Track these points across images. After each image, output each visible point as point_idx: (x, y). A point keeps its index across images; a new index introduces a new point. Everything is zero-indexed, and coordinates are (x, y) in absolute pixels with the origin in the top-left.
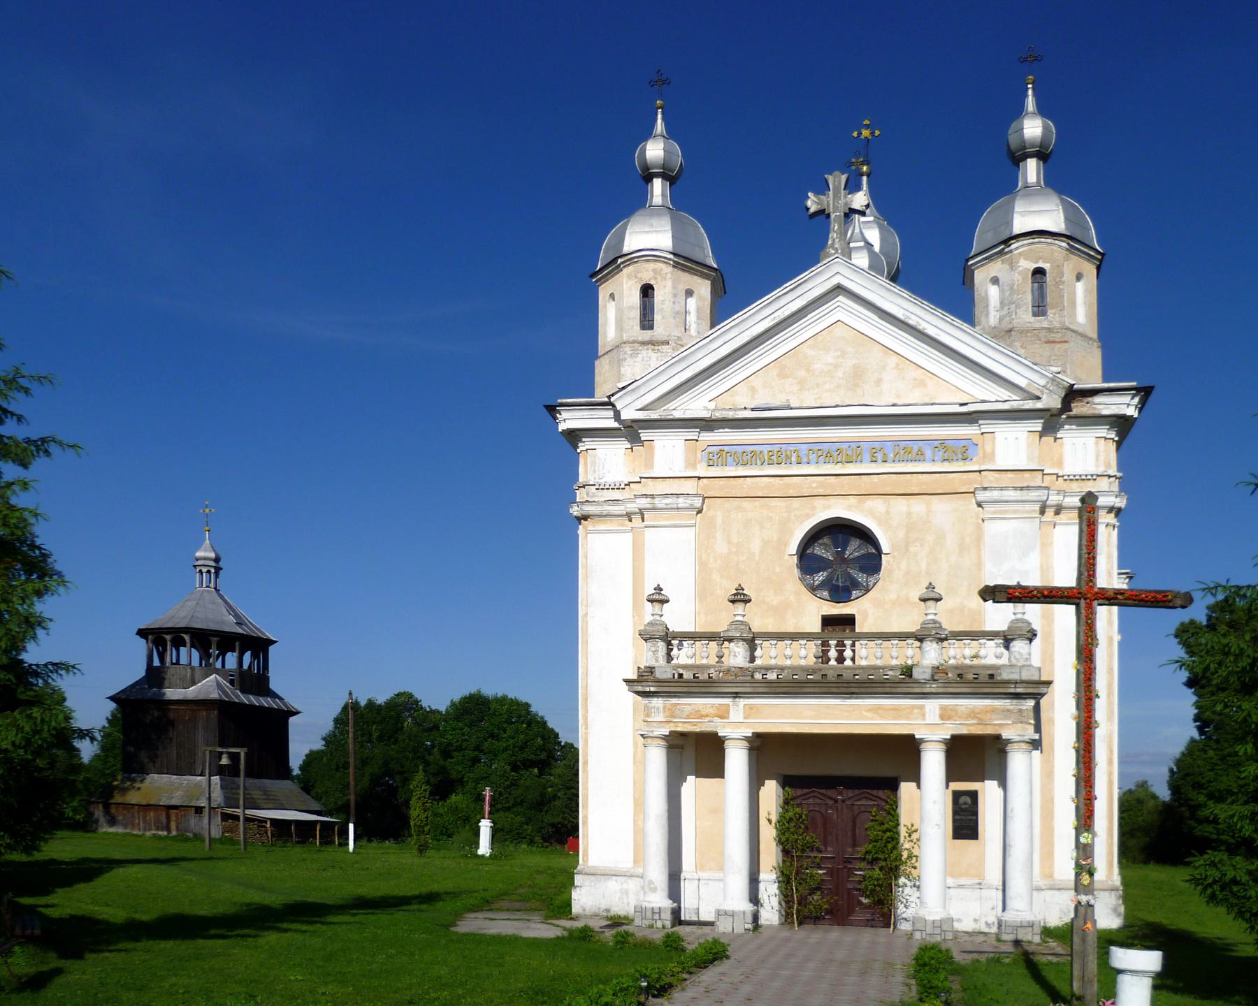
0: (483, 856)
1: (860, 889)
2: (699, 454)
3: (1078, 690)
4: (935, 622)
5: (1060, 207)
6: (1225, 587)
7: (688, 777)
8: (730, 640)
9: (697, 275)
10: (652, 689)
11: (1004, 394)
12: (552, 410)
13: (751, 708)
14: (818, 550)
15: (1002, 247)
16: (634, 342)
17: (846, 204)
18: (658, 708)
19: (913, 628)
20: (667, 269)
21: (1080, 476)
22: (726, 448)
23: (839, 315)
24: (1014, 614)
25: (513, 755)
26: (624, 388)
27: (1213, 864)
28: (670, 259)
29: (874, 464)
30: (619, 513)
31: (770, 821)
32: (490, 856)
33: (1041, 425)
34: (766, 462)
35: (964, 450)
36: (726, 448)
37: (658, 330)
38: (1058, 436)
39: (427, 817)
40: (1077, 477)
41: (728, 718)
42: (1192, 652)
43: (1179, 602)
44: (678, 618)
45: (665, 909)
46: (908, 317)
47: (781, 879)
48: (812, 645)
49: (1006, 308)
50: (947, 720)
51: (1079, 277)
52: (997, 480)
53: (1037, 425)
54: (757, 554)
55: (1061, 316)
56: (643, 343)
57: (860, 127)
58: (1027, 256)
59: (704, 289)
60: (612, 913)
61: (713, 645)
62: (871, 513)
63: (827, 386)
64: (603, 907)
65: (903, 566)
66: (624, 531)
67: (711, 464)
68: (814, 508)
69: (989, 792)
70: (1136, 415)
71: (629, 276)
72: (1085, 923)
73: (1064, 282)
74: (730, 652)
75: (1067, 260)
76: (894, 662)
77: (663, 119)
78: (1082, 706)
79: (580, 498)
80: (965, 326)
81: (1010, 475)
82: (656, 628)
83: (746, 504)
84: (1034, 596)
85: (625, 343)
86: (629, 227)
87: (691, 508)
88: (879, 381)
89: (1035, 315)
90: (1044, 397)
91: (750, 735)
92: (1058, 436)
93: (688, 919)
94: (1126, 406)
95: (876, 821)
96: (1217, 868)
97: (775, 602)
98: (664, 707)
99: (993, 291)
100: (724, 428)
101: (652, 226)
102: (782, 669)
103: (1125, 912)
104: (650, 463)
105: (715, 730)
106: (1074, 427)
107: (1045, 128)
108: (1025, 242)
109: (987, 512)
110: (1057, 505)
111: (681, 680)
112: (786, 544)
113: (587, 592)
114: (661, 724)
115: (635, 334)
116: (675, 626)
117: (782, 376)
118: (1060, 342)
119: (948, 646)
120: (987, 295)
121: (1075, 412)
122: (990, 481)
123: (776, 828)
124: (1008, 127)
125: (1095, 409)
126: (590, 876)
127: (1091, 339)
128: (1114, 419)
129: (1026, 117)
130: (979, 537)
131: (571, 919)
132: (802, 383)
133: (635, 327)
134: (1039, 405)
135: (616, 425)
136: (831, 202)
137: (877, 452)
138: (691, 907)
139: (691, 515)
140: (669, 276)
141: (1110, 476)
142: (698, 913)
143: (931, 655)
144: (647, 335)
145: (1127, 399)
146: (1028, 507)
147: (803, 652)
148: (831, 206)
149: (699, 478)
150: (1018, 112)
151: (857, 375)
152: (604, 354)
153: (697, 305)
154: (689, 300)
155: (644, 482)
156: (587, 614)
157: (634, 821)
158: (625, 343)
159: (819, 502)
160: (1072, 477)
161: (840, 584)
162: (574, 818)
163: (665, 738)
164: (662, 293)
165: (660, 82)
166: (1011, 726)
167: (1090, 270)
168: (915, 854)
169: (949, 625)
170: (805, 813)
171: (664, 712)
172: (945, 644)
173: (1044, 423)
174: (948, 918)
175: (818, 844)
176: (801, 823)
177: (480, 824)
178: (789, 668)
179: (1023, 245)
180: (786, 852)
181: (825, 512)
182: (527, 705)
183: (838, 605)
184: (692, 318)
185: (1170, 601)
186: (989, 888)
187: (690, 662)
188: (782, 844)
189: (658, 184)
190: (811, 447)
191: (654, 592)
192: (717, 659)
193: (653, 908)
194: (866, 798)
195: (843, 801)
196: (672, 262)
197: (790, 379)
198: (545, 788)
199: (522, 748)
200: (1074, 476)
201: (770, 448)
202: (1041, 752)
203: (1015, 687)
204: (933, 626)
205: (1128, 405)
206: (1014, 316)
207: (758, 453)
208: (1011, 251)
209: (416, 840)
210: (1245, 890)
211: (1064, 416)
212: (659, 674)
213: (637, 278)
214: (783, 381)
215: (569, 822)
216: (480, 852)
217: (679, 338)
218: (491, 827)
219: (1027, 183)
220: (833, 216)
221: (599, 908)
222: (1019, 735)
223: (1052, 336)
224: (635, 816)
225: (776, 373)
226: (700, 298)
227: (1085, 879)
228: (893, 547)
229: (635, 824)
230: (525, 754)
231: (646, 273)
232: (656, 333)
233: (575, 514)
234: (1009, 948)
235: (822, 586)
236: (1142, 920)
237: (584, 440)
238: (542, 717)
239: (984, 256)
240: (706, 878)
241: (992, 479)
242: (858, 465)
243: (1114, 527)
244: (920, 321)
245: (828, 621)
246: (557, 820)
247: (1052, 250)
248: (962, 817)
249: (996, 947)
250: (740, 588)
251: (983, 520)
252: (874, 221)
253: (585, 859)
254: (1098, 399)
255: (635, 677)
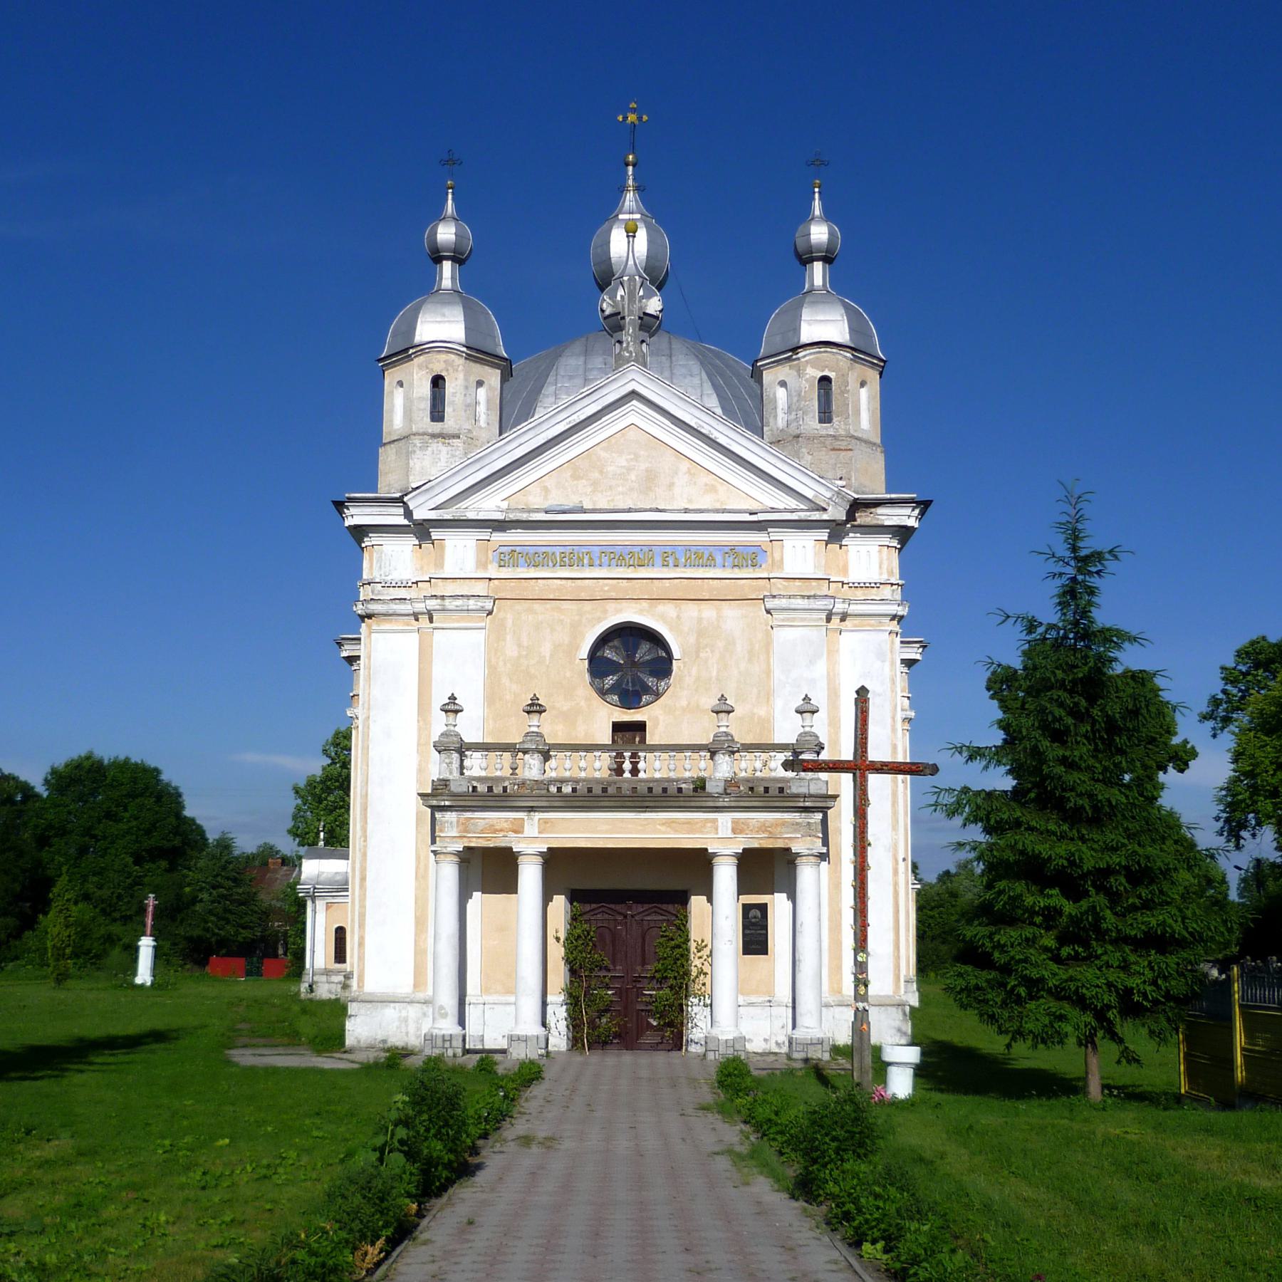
0: (142, 986)
1: (649, 1011)
2: (490, 553)
3: (855, 841)
4: (727, 734)
5: (845, 318)
6: (968, 747)
7: (474, 893)
8: (525, 752)
9: (488, 365)
10: (447, 803)
11: (792, 503)
12: (340, 506)
13: (546, 823)
14: (608, 654)
15: (790, 354)
16: (424, 434)
17: (641, 308)
18: (451, 823)
19: (706, 739)
20: (460, 362)
21: (865, 583)
22: (518, 549)
23: (632, 419)
24: (803, 727)
25: (137, 841)
26: (417, 488)
27: (960, 975)
28: (463, 352)
29: (665, 569)
30: (406, 612)
31: (558, 939)
32: (153, 984)
33: (827, 534)
34: (558, 564)
35: (752, 557)
36: (518, 549)
37: (449, 422)
38: (844, 543)
39: (69, 936)
40: (862, 585)
41: (522, 832)
42: (1006, 707)
43: (928, 771)
44: (470, 728)
45: (456, 1035)
46: (700, 426)
47: (569, 1001)
48: (606, 755)
49: (794, 413)
50: (738, 834)
51: (863, 384)
52: (786, 588)
53: (824, 535)
54: (548, 658)
55: (846, 424)
56: (433, 436)
57: (626, 110)
58: (815, 364)
59: (494, 379)
60: (389, 1044)
61: (507, 755)
62: (663, 618)
63: (620, 489)
64: (380, 1037)
65: (694, 671)
66: (411, 631)
67: (502, 564)
68: (605, 612)
69: (778, 904)
70: (916, 525)
71: (420, 367)
72: (862, 1025)
73: (849, 391)
74: (524, 764)
75: (852, 369)
76: (687, 774)
77: (453, 199)
78: (858, 853)
79: (364, 596)
80: (755, 438)
81: (798, 583)
82: (451, 739)
83: (537, 606)
84: (822, 768)
85: (414, 435)
86: (420, 316)
87: (482, 609)
88: (671, 485)
89: (821, 421)
90: (830, 509)
91: (545, 850)
92: (844, 543)
93: (472, 1047)
94: (906, 517)
95: (666, 936)
96: (964, 979)
97: (565, 708)
98: (458, 822)
99: (781, 393)
100: (516, 529)
101: (444, 315)
102: (577, 781)
103: (912, 1032)
104: (440, 563)
105: (509, 845)
106: (858, 535)
107: (831, 233)
108: (812, 351)
109: (776, 619)
110: (843, 613)
111: (474, 794)
112: (578, 648)
113: (369, 694)
114: (454, 840)
115: (425, 426)
116: (471, 735)
117: (576, 477)
118: (845, 450)
119: (739, 758)
120: (775, 397)
121: (859, 522)
122: (779, 589)
123: (564, 946)
124: (795, 230)
125: (878, 519)
126: (366, 1004)
127: (874, 444)
128: (897, 529)
129: (813, 222)
130: (768, 645)
131: (345, 1052)
132: (595, 484)
133: (425, 419)
134: (825, 517)
135: (406, 522)
136: (626, 306)
137: (668, 556)
138: (476, 1034)
139: (480, 617)
140: (461, 368)
141: (892, 584)
142: (483, 1040)
143: (724, 768)
144: (437, 427)
145: (908, 511)
146: (815, 615)
147: (597, 764)
148: (626, 310)
149: (490, 579)
150: (805, 216)
151: (650, 479)
152: (390, 443)
153: (487, 396)
154: (479, 390)
155: (435, 583)
156: (369, 717)
157: (415, 941)
158: (414, 435)
159: (611, 606)
160: (856, 585)
161: (631, 689)
162: (219, 929)
163: (458, 854)
164: (453, 385)
165: (450, 161)
166: (800, 840)
167: (873, 376)
168: (705, 971)
169: (742, 737)
170: (593, 929)
171: (458, 827)
172: (737, 755)
173: (829, 533)
174: (740, 1038)
175: (607, 962)
176: (590, 940)
177: (140, 943)
178: (584, 780)
179: (811, 354)
180: (573, 972)
181: (618, 615)
182: (157, 771)
183: (629, 711)
184: (482, 409)
185: (922, 771)
186: (779, 1006)
187: (483, 774)
188: (570, 963)
189: (447, 266)
190: (604, 549)
191: (448, 701)
192: (511, 771)
193: (444, 1036)
194: (655, 912)
195: (632, 916)
196: (464, 355)
197: (584, 481)
198: (181, 887)
199: (148, 832)
200: (859, 583)
201: (562, 549)
202: (829, 863)
203: (804, 801)
204: (726, 738)
205: (909, 516)
206: (801, 423)
207: (550, 555)
208: (798, 359)
209: (55, 967)
210: (984, 994)
211: (849, 526)
212: (454, 788)
213: (427, 368)
214: (575, 482)
215: (214, 934)
216: (139, 980)
217: (469, 431)
218: (154, 947)
219: (813, 285)
220: (627, 319)
221: (376, 1039)
222: (808, 849)
223: (837, 444)
224: (416, 935)
225: (569, 474)
226: (491, 388)
227: (862, 990)
228: (684, 653)
229: (415, 945)
230: (152, 840)
231: (438, 363)
232: (446, 426)
233: (359, 612)
234: (799, 1065)
235: (612, 690)
236: (928, 1038)
237: (370, 535)
238: (176, 788)
239: (773, 360)
240: (492, 1002)
241: (780, 586)
242: (649, 569)
243: (897, 634)
244: (713, 430)
245: (618, 727)
246: (197, 932)
247: (838, 359)
248: (753, 931)
249: (787, 1065)
250: (535, 698)
251: (772, 628)
252: (641, 218)
253: (361, 985)
254: (880, 510)
255: (429, 791)
